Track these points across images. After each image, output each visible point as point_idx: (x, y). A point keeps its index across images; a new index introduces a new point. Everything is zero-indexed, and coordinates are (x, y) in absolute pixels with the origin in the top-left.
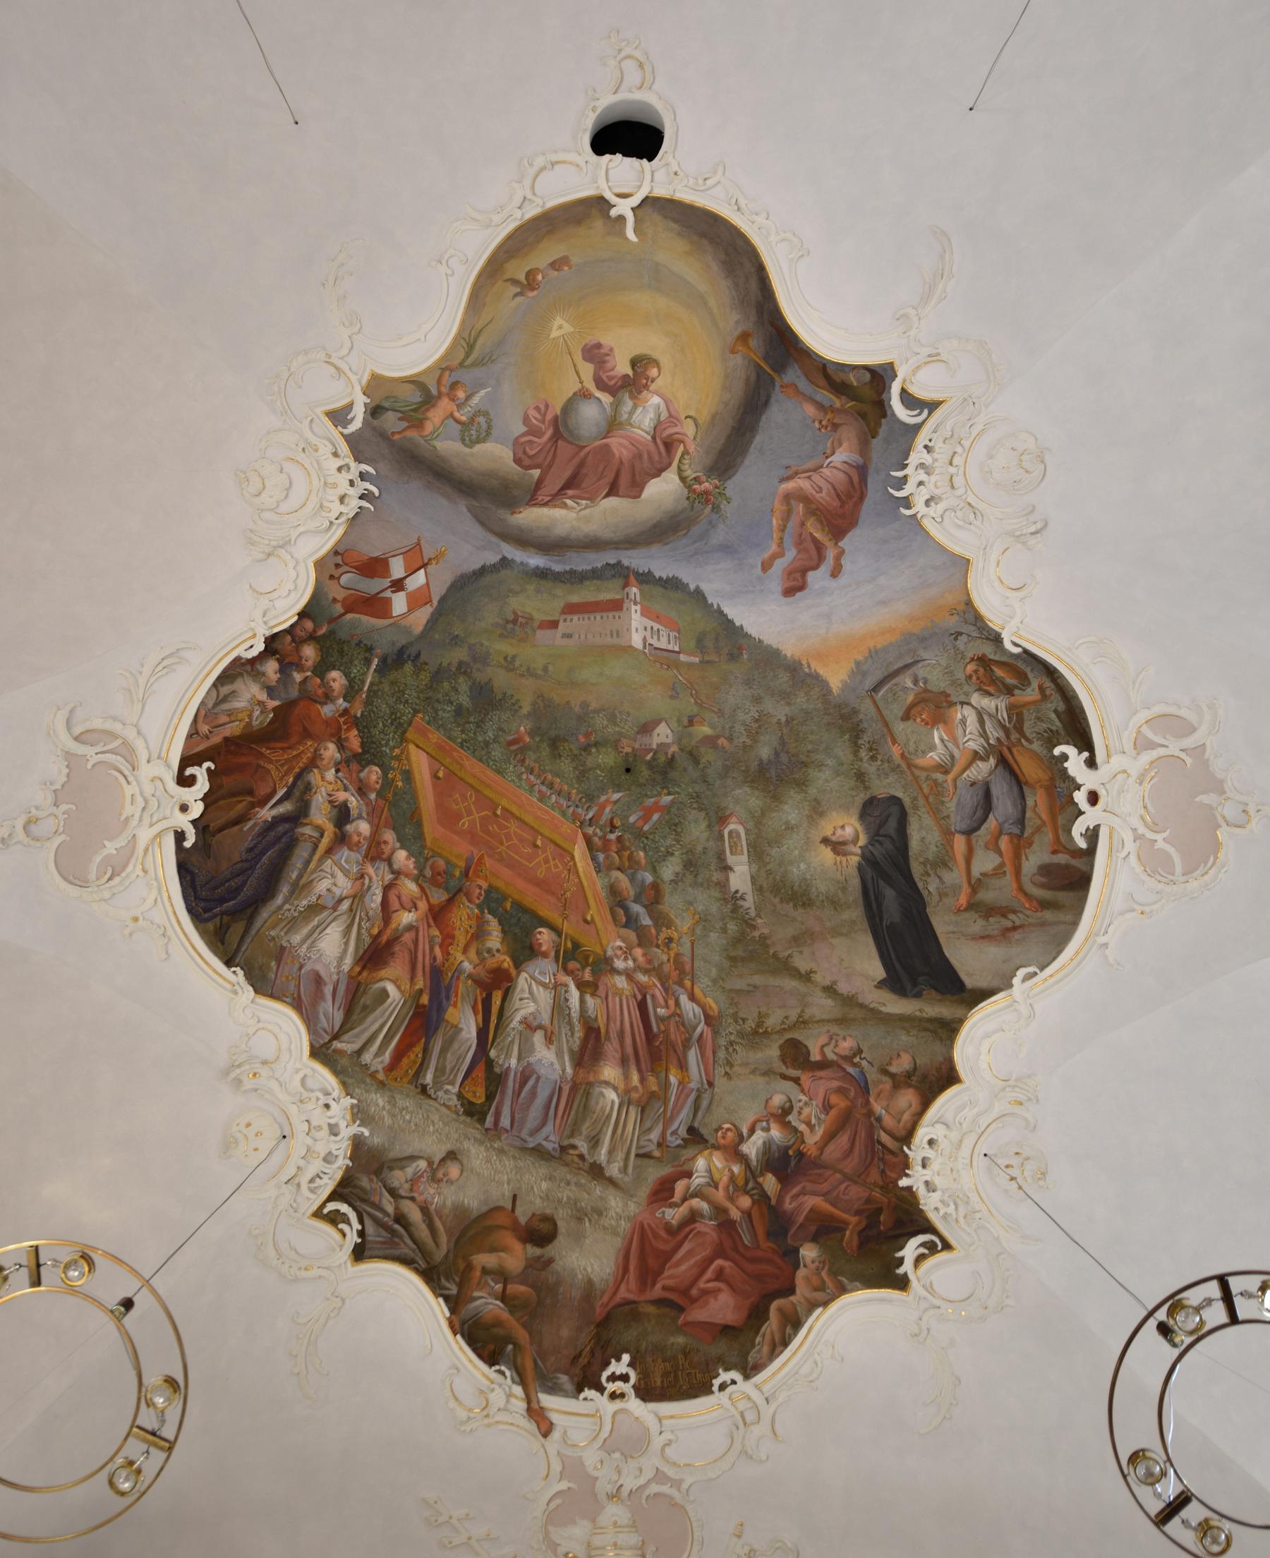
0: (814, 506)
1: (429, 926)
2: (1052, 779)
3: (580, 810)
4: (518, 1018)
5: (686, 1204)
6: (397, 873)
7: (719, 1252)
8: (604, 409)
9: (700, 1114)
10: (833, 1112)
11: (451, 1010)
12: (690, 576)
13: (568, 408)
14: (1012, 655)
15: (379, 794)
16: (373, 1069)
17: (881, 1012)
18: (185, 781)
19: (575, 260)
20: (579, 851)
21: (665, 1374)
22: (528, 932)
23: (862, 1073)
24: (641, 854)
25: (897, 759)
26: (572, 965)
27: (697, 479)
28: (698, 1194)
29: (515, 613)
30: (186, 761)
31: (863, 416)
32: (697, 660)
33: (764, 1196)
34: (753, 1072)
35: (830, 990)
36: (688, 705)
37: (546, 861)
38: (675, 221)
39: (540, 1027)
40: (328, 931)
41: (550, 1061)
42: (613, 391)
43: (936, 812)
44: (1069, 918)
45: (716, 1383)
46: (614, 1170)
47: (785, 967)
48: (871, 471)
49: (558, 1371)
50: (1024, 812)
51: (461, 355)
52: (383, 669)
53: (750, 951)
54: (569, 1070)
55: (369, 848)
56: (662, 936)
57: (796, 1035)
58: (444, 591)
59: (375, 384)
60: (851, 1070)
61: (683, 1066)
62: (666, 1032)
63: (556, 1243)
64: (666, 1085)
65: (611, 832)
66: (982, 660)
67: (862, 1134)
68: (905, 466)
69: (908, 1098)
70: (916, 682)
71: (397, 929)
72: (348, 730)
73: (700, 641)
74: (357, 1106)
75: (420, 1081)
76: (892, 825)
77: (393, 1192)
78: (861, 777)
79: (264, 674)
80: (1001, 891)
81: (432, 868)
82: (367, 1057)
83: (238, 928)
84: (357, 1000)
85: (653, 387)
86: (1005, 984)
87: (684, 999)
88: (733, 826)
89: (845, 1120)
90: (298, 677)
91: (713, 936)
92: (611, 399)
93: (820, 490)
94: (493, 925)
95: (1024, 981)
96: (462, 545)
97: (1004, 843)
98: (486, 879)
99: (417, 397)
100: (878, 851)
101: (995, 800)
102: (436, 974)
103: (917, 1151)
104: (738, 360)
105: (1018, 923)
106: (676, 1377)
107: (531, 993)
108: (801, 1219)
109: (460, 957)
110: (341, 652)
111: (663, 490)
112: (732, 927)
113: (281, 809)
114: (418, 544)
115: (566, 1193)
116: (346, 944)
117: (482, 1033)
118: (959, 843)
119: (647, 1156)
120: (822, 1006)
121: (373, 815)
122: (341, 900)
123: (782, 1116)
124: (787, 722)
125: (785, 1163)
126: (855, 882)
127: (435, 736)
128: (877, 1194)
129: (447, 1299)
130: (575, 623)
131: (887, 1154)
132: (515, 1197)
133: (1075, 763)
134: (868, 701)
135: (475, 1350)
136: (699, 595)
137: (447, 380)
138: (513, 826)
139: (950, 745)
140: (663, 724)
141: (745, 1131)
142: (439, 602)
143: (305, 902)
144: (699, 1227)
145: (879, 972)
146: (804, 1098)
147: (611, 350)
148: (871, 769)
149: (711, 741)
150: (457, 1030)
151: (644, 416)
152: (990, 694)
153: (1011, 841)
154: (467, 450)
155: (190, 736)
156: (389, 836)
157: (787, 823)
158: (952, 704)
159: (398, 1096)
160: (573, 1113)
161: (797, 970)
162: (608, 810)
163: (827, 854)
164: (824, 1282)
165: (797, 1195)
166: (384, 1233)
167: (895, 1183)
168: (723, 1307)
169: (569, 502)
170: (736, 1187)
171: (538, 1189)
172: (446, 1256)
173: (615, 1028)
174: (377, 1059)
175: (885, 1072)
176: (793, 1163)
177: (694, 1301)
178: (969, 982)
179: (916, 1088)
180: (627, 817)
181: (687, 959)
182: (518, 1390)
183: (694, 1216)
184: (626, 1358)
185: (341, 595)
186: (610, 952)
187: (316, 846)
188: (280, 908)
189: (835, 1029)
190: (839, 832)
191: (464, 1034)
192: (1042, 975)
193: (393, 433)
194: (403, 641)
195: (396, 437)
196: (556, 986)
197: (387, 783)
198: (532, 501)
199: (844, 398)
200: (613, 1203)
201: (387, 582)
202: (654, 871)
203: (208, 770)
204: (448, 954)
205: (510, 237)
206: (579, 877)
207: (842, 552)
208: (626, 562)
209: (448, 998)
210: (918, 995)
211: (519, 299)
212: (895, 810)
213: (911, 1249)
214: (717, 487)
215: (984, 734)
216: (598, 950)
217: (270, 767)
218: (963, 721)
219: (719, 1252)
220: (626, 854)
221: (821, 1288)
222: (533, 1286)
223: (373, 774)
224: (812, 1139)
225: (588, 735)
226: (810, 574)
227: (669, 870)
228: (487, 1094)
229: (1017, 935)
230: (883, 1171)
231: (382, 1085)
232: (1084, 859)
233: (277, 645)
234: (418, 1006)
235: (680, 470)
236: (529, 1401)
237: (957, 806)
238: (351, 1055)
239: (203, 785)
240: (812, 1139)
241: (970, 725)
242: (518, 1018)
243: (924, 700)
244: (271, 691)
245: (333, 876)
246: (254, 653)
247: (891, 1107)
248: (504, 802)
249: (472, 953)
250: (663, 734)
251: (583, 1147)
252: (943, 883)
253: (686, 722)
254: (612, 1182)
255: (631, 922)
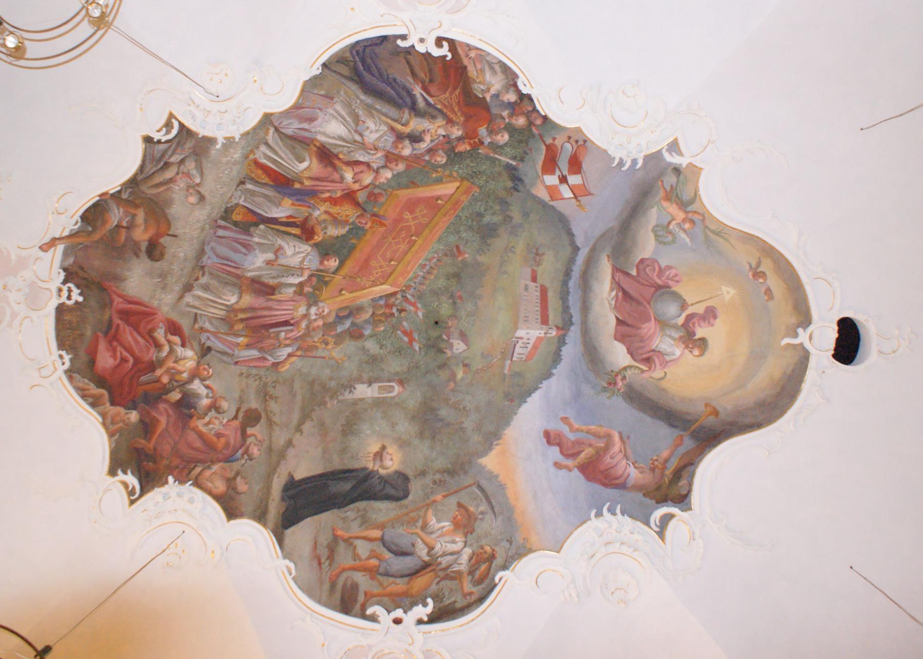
0: (601, 453)
1: (343, 190)
2: (412, 596)
3: (412, 290)
4: (283, 244)
5: (166, 343)
6: (377, 171)
7: (137, 361)
8: (672, 319)
9: (219, 355)
10: (215, 439)
11: (290, 202)
12: (561, 370)
13: (676, 296)
14: (494, 576)
15: (429, 162)
16: (256, 151)
17: (274, 474)
18: (439, 41)
19: (770, 304)
20: (386, 288)
21: (70, 322)
22: (337, 253)
23: (238, 459)
24: (382, 329)
25: (433, 498)
26: (314, 280)
27: (624, 378)
28: (172, 351)
29: (543, 254)
30: (452, 43)
31: (658, 488)
32: (506, 372)
33: (168, 391)
34: (242, 391)
35: (289, 443)
36: (477, 364)
37: (381, 267)
38: (793, 371)
39: (277, 258)
40: (342, 126)
41: (256, 263)
42: (685, 325)
43: (396, 521)
44: (324, 599)
45: (63, 353)
46: (188, 299)
47: (305, 416)
48: (621, 491)
49: (76, 257)
50: (392, 576)
51: (713, 227)
52: (510, 169)
53: (318, 394)
54: (249, 274)
55: (394, 154)
56: (330, 339)
57: (263, 420)
58: (559, 209)
59: (695, 170)
60: (240, 452)
61: (248, 346)
62: (269, 337)
63: (147, 260)
64: (238, 336)
65: (398, 310)
66: (493, 557)
67: (201, 456)
68: (623, 514)
69: (220, 486)
70: (482, 513)
71: (342, 169)
72: (470, 144)
73: (519, 374)
74: (234, 142)
75: (247, 181)
76: (390, 491)
77: (182, 162)
78: (423, 473)
79: (507, 92)
80: (344, 558)
81: (380, 194)
82: (263, 148)
83: (345, 71)
84: (300, 143)
85: (687, 352)
86: (287, 556)
87: (289, 350)
88: (397, 389)
89: (209, 445)
90: (505, 113)
91: (328, 372)
92: (680, 324)
93: (612, 458)
94: (342, 231)
95: (287, 567)
96: (590, 221)
97: (374, 562)
98: (371, 228)
99: (686, 197)
100: (375, 481)
101: (401, 558)
102: (312, 193)
103: (189, 489)
104: (700, 408)
105: (323, 566)
106: (68, 329)
107: (298, 253)
108: (154, 414)
109: (323, 208)
110: (520, 141)
111: (618, 355)
112: (333, 384)
113: (420, 100)
114: (590, 194)
115: (176, 267)
116: (334, 138)
117: (275, 221)
118: (376, 533)
119: (195, 320)
120: (280, 438)
121: (415, 158)
122: (361, 135)
123: (214, 406)
124: (462, 428)
125: (186, 407)
126: (356, 465)
127: (465, 199)
128: (166, 462)
129: (119, 192)
130: (535, 294)
131: (186, 470)
132: (175, 236)
133: (421, 611)
134: (472, 482)
135: (90, 208)
136: (549, 375)
137: (696, 218)
138: (403, 247)
139: (439, 532)
140: (465, 347)
141: (207, 382)
142: (553, 207)
143: (361, 113)
144: (153, 349)
145: (298, 476)
146: (225, 421)
147: (712, 325)
148: (428, 480)
149: (454, 375)
150: (278, 205)
151: (667, 344)
152: (470, 560)
153: (375, 566)
154: (650, 228)
155: (468, 45)
156: (401, 167)
157: (397, 424)
158: (466, 535)
159: (238, 167)
160: (224, 275)
161: (303, 423)
162: (412, 308)
163: (375, 448)
164: (117, 424)
165: (167, 413)
166: (159, 155)
167: (171, 473)
168: (106, 360)
169: (614, 293)
170: (174, 374)
171: (180, 251)
172: (143, 193)
173: (274, 305)
174: (262, 155)
175: (238, 474)
176: (186, 411)
177: (110, 343)
178: (289, 532)
179: (226, 493)
180: (406, 320)
181: (314, 354)
182: (66, 233)
183: (158, 346)
184: (80, 299)
185: (558, 143)
186: (321, 304)
187: (396, 121)
188: (358, 97)
189: (266, 444)
190: (389, 457)
191: (274, 209)
192: (289, 578)
193: (662, 181)
194: (527, 180)
195: (660, 183)
196: (302, 269)
197: (435, 168)
198: (616, 269)
199: (671, 476)
200: (169, 297)
201: (565, 172)
202: (371, 336)
203: (446, 56)
204: (325, 201)
205: (788, 262)
206: (370, 287)
207: (570, 470)
208: (573, 328)
209: (297, 200)
210: (283, 499)
211: (748, 267)
212: (401, 494)
213: (132, 480)
214: (619, 390)
215: (444, 554)
216: (323, 297)
217: (447, 94)
218: (454, 542)
219: (137, 361)
220: (383, 319)
221: (113, 423)
222: (124, 245)
223: (441, 159)
224: (200, 424)
225: (461, 298)
226: (557, 449)
227: (371, 346)
228: (242, 222)
229: (315, 564)
230: (177, 467)
231: (247, 157)
232: (360, 612)
233: (526, 101)
234: (294, 181)
235: (631, 367)
236: (59, 239)
237: (401, 535)
238: (264, 138)
239: (436, 52)
240: (200, 424)
241: (449, 544)
242: (283, 244)
243: (469, 516)
244: (496, 96)
245: (377, 131)
246: (521, 87)
247: (215, 475)
248: (419, 242)
249: (324, 217)
250: (459, 346)
251: (203, 280)
252: (352, 521)
253: (466, 362)
254: (181, 297)
255: (340, 319)
